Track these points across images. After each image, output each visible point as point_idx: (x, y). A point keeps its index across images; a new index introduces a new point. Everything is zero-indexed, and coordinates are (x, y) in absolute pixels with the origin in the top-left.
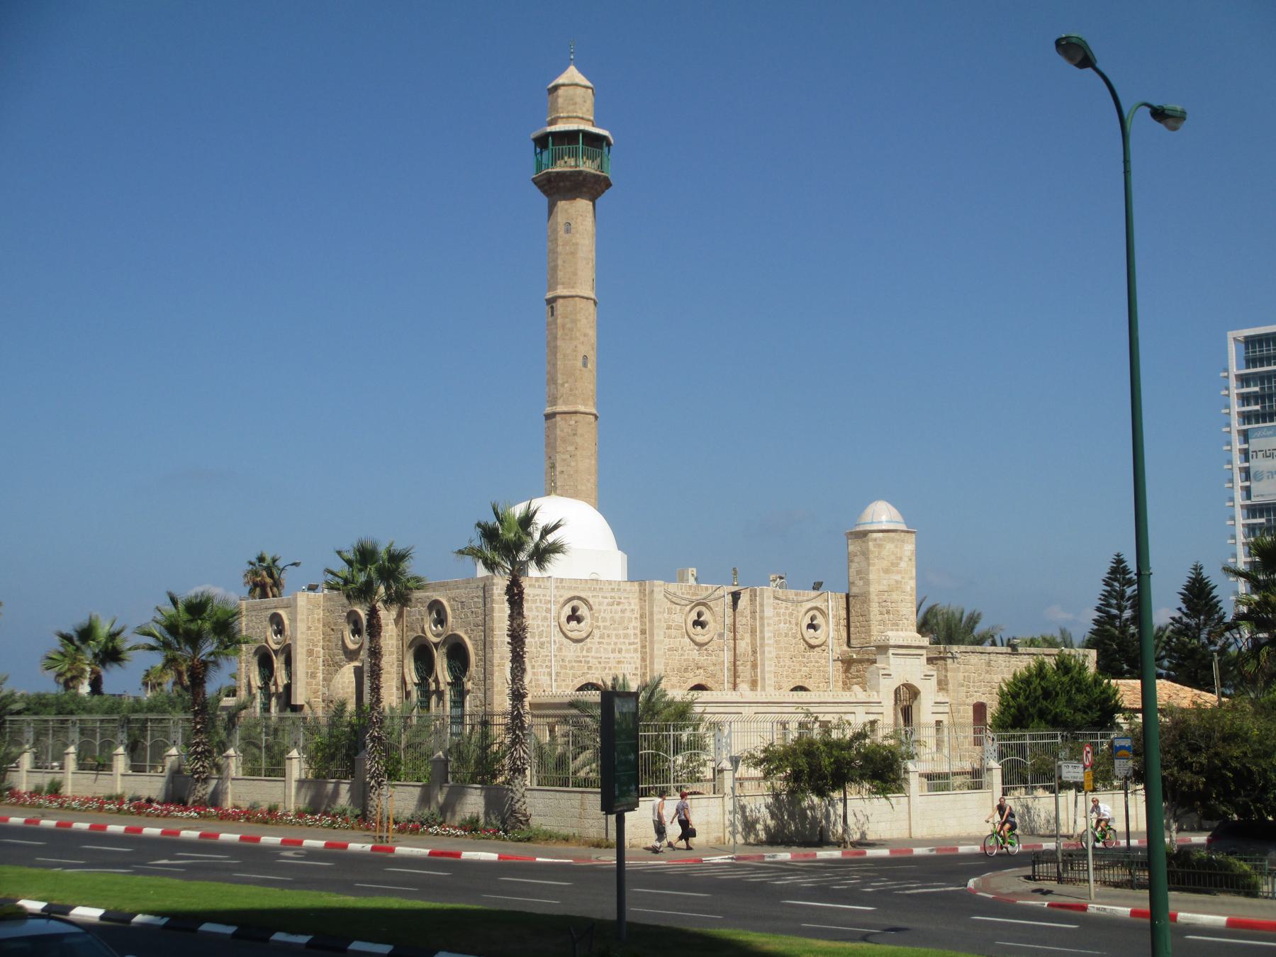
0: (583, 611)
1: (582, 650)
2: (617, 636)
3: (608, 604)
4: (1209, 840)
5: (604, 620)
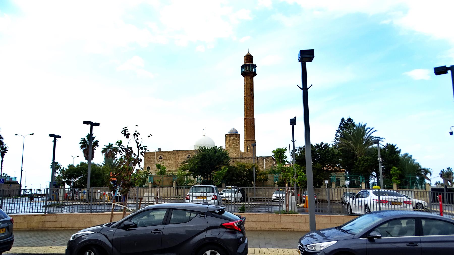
0: (162, 157)
4: (241, 151)
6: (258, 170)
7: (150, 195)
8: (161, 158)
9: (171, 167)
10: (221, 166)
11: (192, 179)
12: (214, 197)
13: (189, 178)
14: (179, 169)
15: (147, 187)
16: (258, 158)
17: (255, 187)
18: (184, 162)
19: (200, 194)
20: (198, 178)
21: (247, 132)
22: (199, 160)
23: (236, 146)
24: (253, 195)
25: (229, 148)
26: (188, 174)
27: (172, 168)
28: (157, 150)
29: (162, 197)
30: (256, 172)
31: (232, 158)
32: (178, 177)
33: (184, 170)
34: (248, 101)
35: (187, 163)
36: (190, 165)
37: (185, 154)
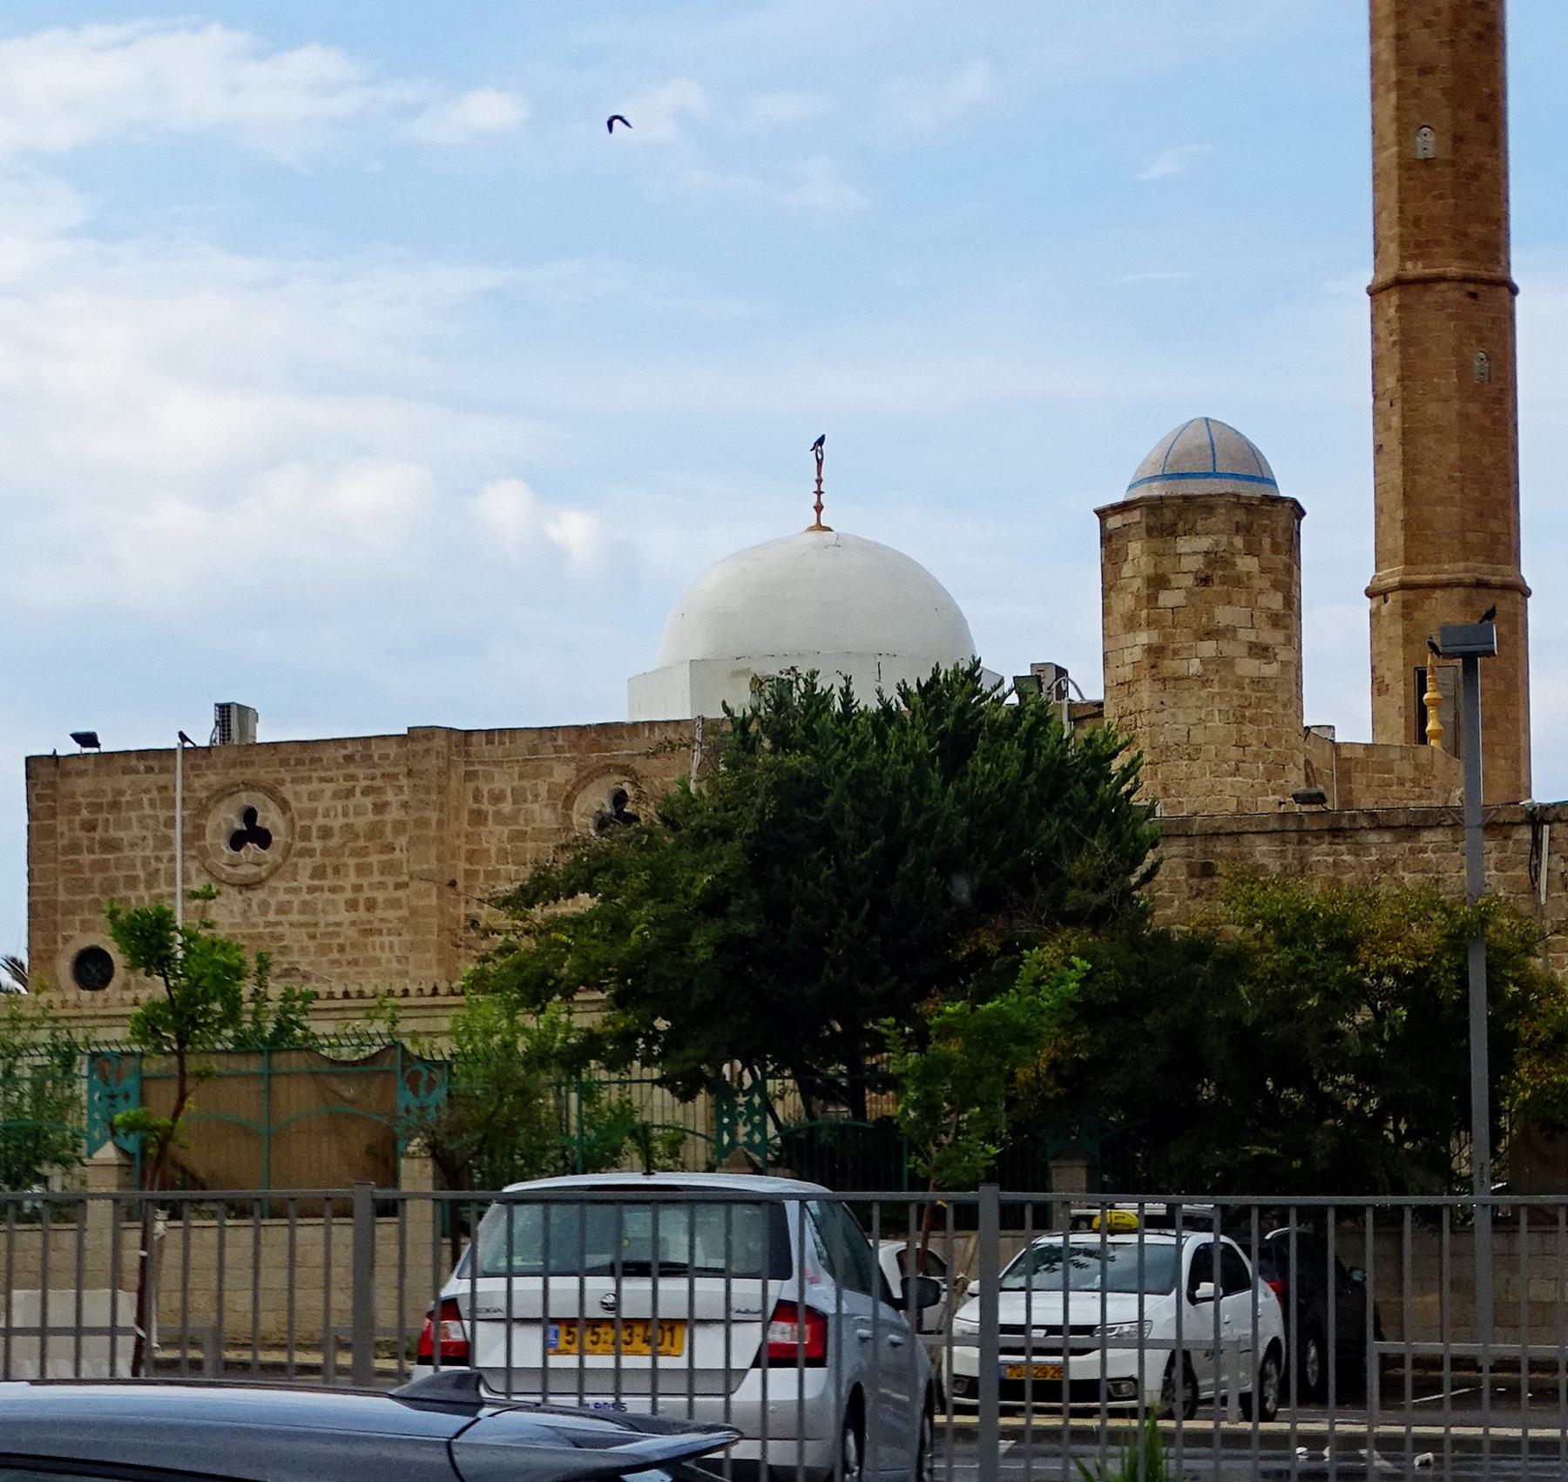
0: (270, 818)
1: (264, 906)
2: (362, 870)
3: (335, 795)
4: (1321, 737)
5: (326, 833)
6: (1528, 985)
7: (97, 1310)
8: (251, 833)
9: (386, 949)
10: (1023, 927)
11: (658, 1106)
12: (782, 1333)
13: (610, 1097)
14: (479, 982)
15: (68, 1209)
16: (1538, 817)
17: (1484, 1196)
18: (539, 889)
19: (601, 1286)
20: (723, 1093)
21: (1410, 466)
22: (730, 855)
23: (1248, 667)
24: (1463, 1325)
25: (1146, 694)
26: (591, 1045)
27: (375, 961)
28: (203, 734)
29: (256, 1341)
30: (1504, 1010)
31: (1179, 830)
32: (474, 1083)
33: (536, 988)
34: (1426, 43)
35: (585, 902)
36: (619, 926)
37: (562, 774)
